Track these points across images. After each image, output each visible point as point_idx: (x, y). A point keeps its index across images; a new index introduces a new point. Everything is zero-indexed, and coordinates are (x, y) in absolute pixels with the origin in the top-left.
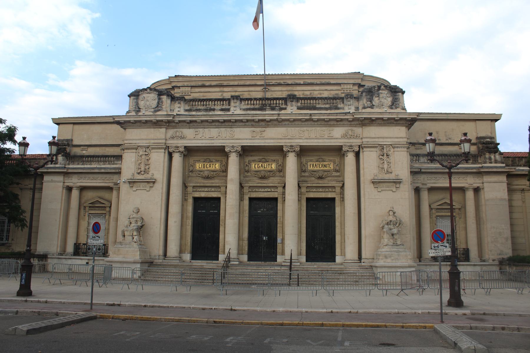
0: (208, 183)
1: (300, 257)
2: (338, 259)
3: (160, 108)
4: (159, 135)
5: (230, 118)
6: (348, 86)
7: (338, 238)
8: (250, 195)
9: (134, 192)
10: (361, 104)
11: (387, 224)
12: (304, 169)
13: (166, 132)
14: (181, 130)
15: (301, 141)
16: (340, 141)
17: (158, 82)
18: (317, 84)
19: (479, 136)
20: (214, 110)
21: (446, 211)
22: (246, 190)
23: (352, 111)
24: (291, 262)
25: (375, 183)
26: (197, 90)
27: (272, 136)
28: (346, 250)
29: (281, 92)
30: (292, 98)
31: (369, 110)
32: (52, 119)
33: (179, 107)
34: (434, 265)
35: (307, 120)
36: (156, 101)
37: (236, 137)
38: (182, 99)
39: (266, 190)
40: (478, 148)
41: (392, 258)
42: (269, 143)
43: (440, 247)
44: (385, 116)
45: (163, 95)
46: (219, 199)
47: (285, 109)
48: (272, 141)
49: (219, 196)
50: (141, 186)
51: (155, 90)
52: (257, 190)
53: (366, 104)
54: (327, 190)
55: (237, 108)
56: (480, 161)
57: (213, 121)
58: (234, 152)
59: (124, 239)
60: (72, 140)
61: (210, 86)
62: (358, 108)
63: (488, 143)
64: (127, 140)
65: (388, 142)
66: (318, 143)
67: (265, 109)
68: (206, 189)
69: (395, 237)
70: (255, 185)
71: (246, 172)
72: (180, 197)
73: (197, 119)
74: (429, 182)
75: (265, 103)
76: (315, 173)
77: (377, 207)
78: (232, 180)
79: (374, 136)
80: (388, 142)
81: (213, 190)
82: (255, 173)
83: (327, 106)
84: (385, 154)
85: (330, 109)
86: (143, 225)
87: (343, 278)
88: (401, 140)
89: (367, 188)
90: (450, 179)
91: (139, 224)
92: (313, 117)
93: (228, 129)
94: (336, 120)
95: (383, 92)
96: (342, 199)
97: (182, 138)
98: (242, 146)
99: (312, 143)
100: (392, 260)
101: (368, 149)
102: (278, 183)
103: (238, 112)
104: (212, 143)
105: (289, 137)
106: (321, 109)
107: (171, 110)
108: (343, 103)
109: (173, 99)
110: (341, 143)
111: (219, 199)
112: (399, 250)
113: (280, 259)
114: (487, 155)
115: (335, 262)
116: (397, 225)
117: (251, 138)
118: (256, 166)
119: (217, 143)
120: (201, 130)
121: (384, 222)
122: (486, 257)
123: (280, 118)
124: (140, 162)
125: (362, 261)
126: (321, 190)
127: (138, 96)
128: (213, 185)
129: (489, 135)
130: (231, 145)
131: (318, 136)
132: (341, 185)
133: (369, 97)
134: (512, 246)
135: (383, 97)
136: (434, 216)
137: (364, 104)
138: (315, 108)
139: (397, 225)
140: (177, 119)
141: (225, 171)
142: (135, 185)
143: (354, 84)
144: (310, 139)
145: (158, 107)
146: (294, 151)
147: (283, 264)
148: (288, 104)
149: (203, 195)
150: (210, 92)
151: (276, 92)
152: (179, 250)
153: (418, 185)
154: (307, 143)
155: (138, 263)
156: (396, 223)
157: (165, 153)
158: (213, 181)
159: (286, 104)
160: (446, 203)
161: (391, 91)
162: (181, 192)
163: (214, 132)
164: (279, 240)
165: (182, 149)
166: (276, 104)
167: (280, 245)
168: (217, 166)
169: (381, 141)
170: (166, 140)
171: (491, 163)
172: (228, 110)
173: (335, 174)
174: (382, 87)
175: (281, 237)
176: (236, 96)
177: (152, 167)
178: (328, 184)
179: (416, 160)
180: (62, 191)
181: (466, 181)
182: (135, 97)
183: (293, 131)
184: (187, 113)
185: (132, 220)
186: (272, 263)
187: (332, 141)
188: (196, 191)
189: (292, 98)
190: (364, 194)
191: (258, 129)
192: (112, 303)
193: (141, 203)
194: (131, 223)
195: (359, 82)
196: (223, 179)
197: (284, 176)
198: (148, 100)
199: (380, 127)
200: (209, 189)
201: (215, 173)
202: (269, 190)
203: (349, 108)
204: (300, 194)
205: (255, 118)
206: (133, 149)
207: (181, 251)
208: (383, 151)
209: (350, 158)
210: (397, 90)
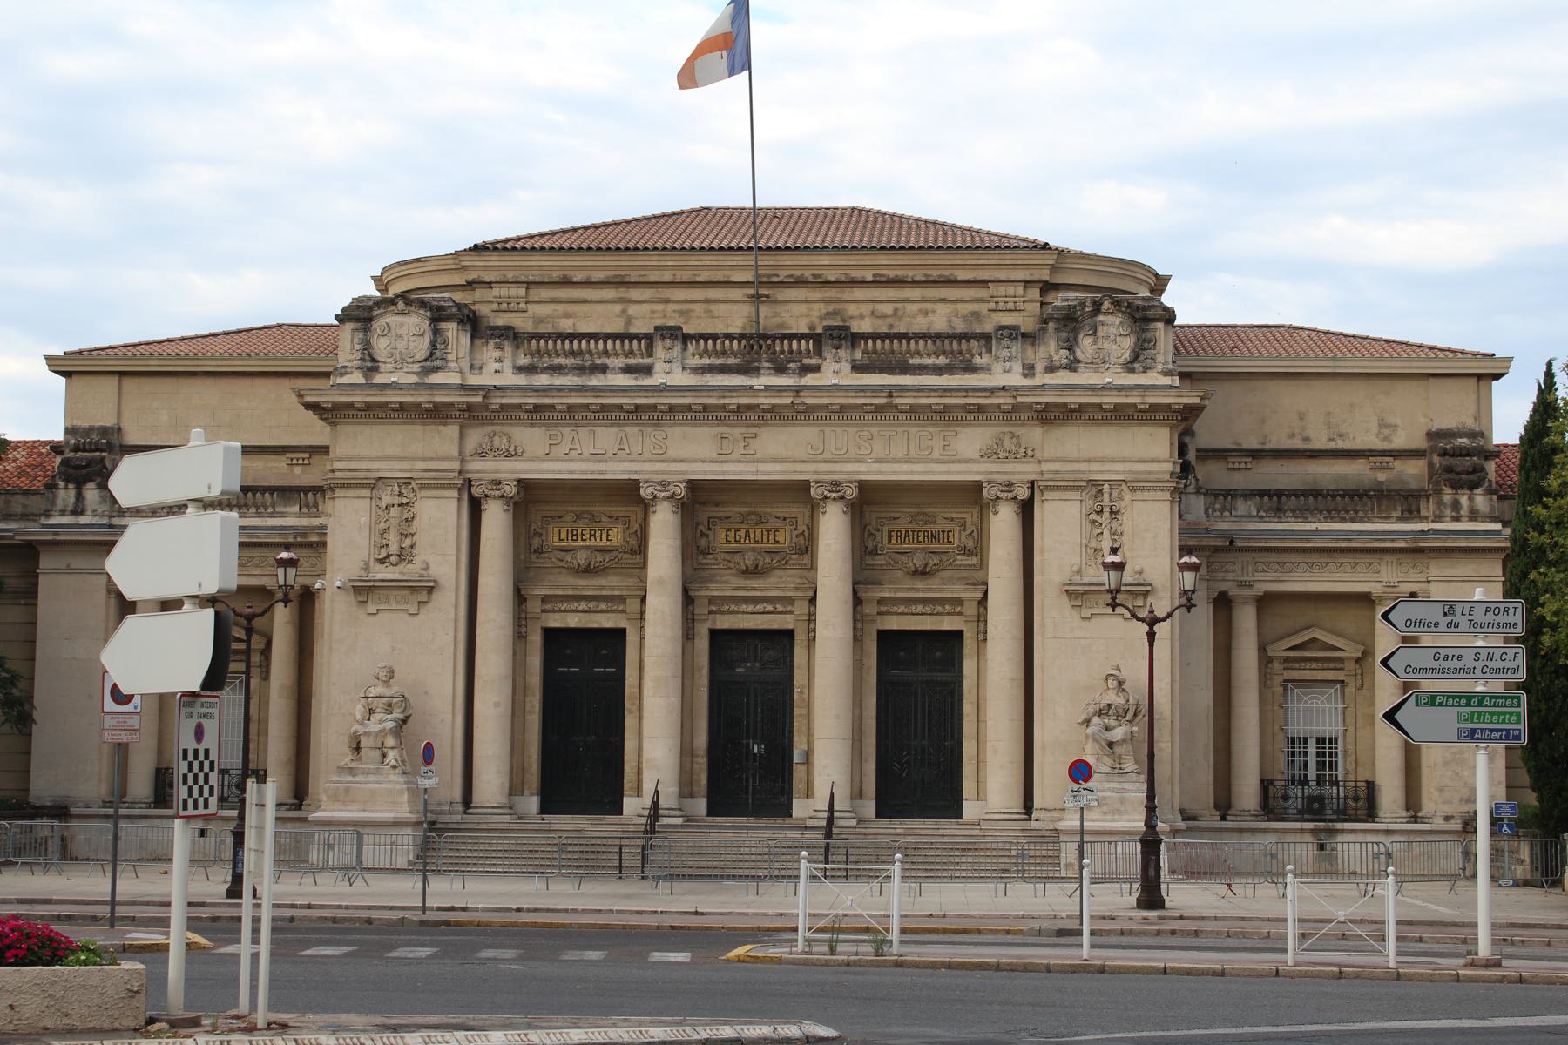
0: (589, 585)
2: (970, 809)
3: (438, 363)
4: (438, 446)
6: (1011, 291)
7: (969, 748)
9: (372, 619)
10: (1039, 356)
11: (1100, 713)
12: (871, 546)
13: (462, 436)
14: (506, 429)
15: (862, 467)
17: (418, 260)
18: (915, 283)
19: (1436, 426)
20: (604, 369)
23: (1015, 379)
24: (830, 820)
25: (1077, 594)
26: (546, 293)
27: (776, 455)
28: (990, 787)
30: (841, 336)
32: (48, 358)
33: (499, 360)
35: (878, 409)
36: (428, 338)
37: (671, 453)
38: (508, 335)
39: (760, 607)
40: (1431, 465)
41: (1105, 808)
42: (769, 473)
44: (1105, 400)
45: (448, 318)
46: (620, 633)
47: (816, 369)
48: (778, 467)
49: (622, 625)
51: (423, 304)
53: (1056, 358)
55: (674, 365)
56: (1424, 513)
57: (604, 408)
58: (665, 498)
61: (587, 283)
62: (1032, 367)
64: (340, 460)
66: (912, 473)
68: (583, 606)
69: (1118, 750)
70: (728, 593)
71: (703, 553)
72: (509, 630)
73: (555, 401)
74: (1259, 576)
75: (758, 348)
76: (904, 559)
77: (1075, 663)
78: (660, 582)
79: (1074, 454)
80: (1116, 471)
81: (603, 606)
82: (728, 557)
83: (942, 361)
84: (1107, 510)
88: (1155, 467)
89: (1051, 610)
91: (397, 714)
92: (898, 401)
94: (966, 408)
97: (511, 455)
98: (689, 481)
101: (1057, 495)
103: (680, 378)
104: (601, 472)
105: (827, 456)
108: (989, 351)
109: (472, 322)
110: (978, 473)
111: (620, 633)
112: (1126, 786)
113: (800, 808)
114: (1448, 495)
116: (1129, 716)
117: (714, 456)
118: (731, 534)
119: (617, 471)
120: (566, 430)
121: (1091, 710)
122: (1428, 807)
124: (383, 525)
126: (920, 608)
127: (370, 320)
128: (604, 593)
129: (1470, 423)
130: (660, 477)
132: (980, 595)
133: (1065, 335)
136: (1277, 680)
138: (906, 369)
139: (1129, 716)
140: (497, 401)
141: (641, 549)
143: (1027, 284)
145: (434, 359)
146: (842, 498)
147: (810, 823)
148: (825, 354)
149: (573, 621)
150: (585, 302)
152: (507, 785)
153: (1223, 587)
154: (879, 473)
158: (601, 581)
159: (819, 354)
160: (1314, 640)
165: (510, 490)
166: (791, 352)
167: (803, 768)
168: (616, 535)
169: (1097, 472)
170: (463, 461)
171: (1457, 519)
172: (648, 370)
173: (962, 560)
174: (1106, 305)
177: (422, 541)
178: (940, 591)
179: (1223, 509)
180: (107, 604)
182: (358, 325)
183: (840, 437)
184: (521, 380)
186: (779, 820)
188: (553, 611)
189: (841, 336)
193: (393, 649)
194: (371, 711)
195: (1046, 278)
196: (632, 576)
197: (813, 567)
198: (400, 336)
200: (592, 605)
201: (607, 557)
202: (770, 608)
203: (1003, 373)
205: (727, 401)
206: (363, 486)
207: (515, 789)
208: (1101, 498)
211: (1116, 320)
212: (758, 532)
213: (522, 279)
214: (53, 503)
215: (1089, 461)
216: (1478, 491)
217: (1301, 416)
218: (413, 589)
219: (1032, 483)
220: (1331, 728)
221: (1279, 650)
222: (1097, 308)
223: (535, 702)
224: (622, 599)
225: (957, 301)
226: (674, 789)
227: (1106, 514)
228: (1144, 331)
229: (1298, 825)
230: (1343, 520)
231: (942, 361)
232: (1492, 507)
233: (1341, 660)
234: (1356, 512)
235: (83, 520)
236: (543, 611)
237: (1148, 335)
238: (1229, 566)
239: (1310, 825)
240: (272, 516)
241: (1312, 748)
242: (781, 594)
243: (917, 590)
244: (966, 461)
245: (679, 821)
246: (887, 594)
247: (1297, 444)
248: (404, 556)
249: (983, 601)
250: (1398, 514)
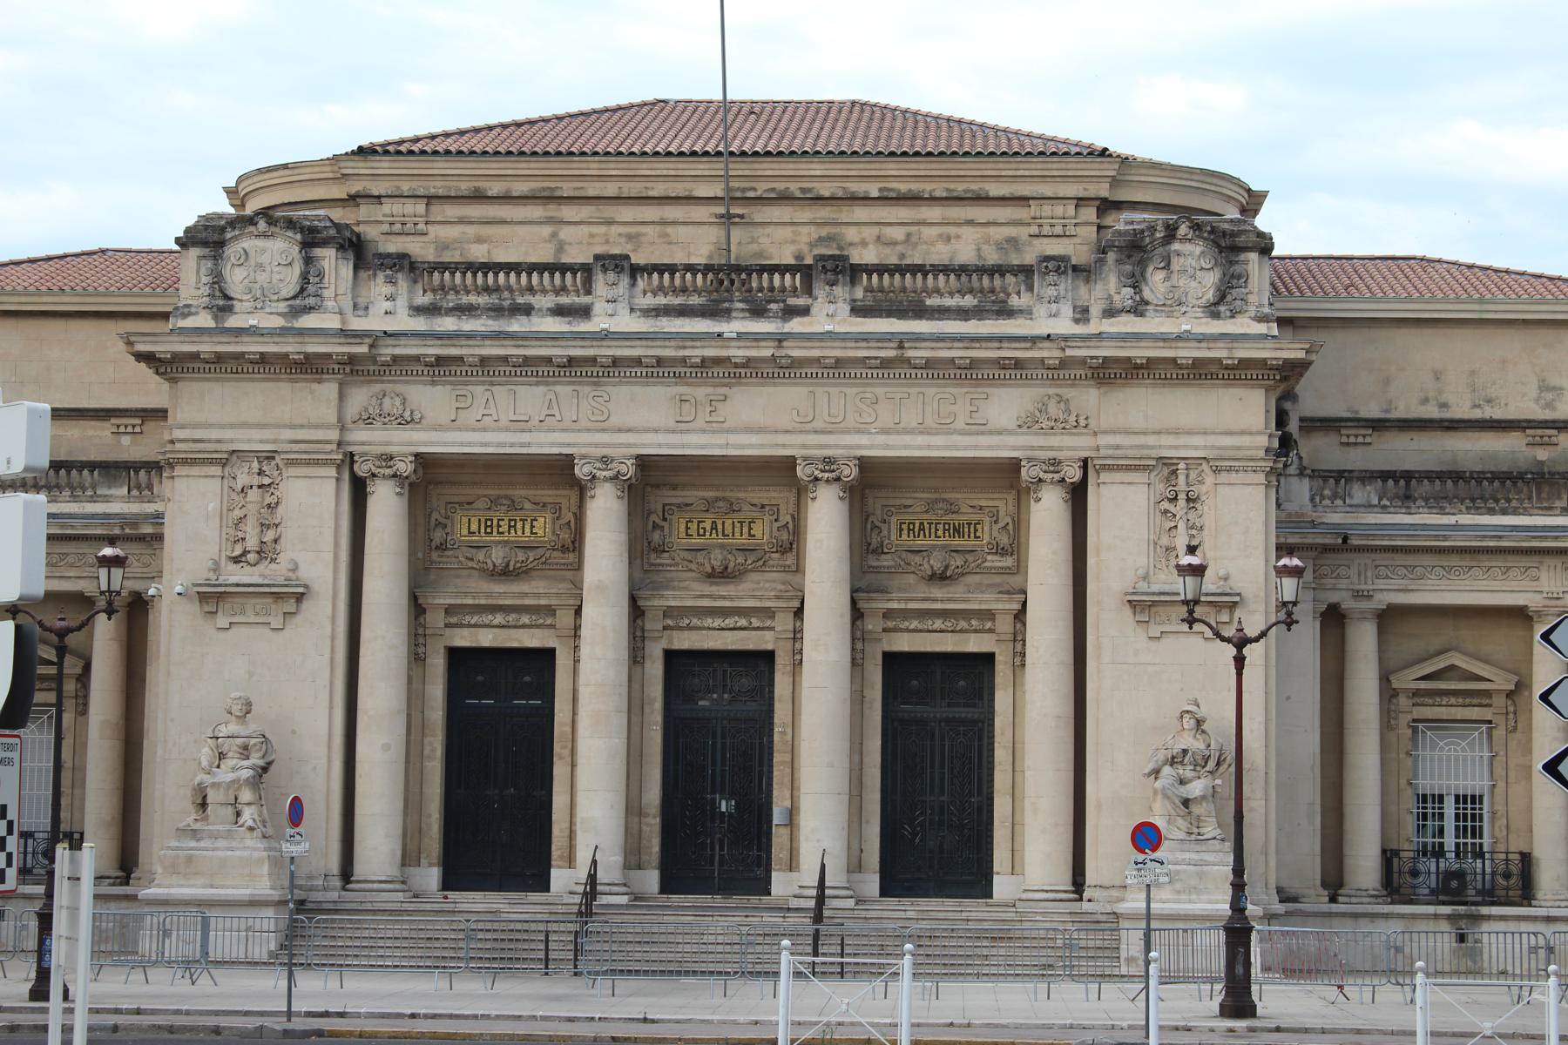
0: (506, 592)
1: (857, 876)
2: (1002, 886)
3: (311, 301)
4: (312, 408)
6: (1059, 210)
8: (671, 642)
9: (222, 635)
11: (1172, 761)
12: (875, 541)
13: (342, 397)
14: (400, 388)
15: (864, 440)
16: (1011, 440)
17: (285, 166)
18: (933, 199)
20: (527, 310)
21: (1453, 700)
22: (652, 624)
23: (1063, 325)
24: (821, 899)
25: (1142, 606)
26: (452, 211)
27: (752, 422)
28: (1028, 855)
31: (1126, 324)
34: (1387, 916)
35: (885, 363)
36: (297, 269)
37: (615, 420)
39: (729, 622)
41: (1178, 886)
42: (743, 447)
43: (1150, 864)
45: (324, 243)
47: (805, 311)
48: (754, 439)
49: (550, 644)
50: (250, 611)
51: (291, 224)
52: (695, 622)
53: (1116, 298)
54: (963, 624)
57: (527, 361)
58: (606, 479)
59: (206, 819)
61: (506, 198)
62: (1086, 310)
64: (182, 427)
65: (1196, 448)
66: (929, 447)
67: (728, 311)
68: (499, 619)
69: (1196, 809)
70: (689, 603)
74: (1380, 584)
76: (918, 559)
78: (601, 587)
80: (1194, 446)
81: (525, 619)
82: (689, 556)
83: (969, 301)
84: (1182, 496)
85: (977, 313)
86: (269, 763)
89: (1109, 624)
91: (256, 760)
92: (910, 353)
93: (587, 389)
95: (1186, 248)
96: (1018, 660)
98: (638, 457)
99: (906, 447)
100: (1179, 892)
101: (1118, 476)
102: (778, 598)
103: (626, 322)
104: (522, 445)
105: (818, 424)
106: (942, 313)
107: (355, 306)
108: (1030, 288)
109: (355, 248)
110: (1014, 448)
113: (781, 884)
115: (991, 896)
116: (1211, 765)
117: (671, 424)
118: (693, 526)
119: (545, 443)
121: (1161, 756)
123: (782, 353)
124: (238, 513)
125: (1086, 895)
126: (938, 624)
127: (221, 244)
128: (527, 602)
131: (930, 421)
132: (1017, 606)
133: (1128, 268)
136: (1404, 719)
137: (1110, 298)
139: (1211, 765)
140: (387, 351)
141: (575, 544)
142: (226, 605)
143: (1080, 201)
144: (898, 433)
145: (305, 296)
146: (838, 479)
147: (794, 903)
148: (816, 292)
149: (486, 639)
151: (769, 230)
152: (399, 853)
153: (1334, 597)
154: (887, 447)
156: (1207, 760)
157: (338, 480)
159: (809, 291)
160: (1452, 668)
161: (1218, 246)
162: (405, 631)
163: (530, 398)
164: (778, 817)
166: (772, 289)
168: (543, 527)
169: (1168, 446)
170: (343, 429)
173: (994, 561)
174: (1183, 229)
175: (788, 803)
176: (614, 257)
177: (289, 534)
179: (1334, 497)
181: (1533, 585)
183: (835, 400)
184: (420, 324)
185: (227, 745)
186: (754, 900)
190: (1098, 647)
191: (701, 393)
193: (251, 674)
196: (563, 580)
197: (799, 569)
198: (260, 267)
199: (1166, 390)
200: (512, 618)
201: (531, 555)
202: (743, 622)
203: (1048, 317)
205: (687, 353)
206: (211, 462)
207: (409, 857)
209: (1047, 515)
211: (1197, 248)
212: (728, 523)
213: (421, 192)
218: (278, 597)
219: (1085, 462)
221: (1406, 680)
222: (1171, 233)
223: (436, 745)
224: (550, 610)
225: (988, 224)
227: (1182, 502)
228: (1232, 263)
229: (1430, 909)
230: (1492, 512)
231: (969, 301)
234: (1509, 501)
236: (447, 626)
237: (1237, 269)
239: (1447, 910)
240: (92, 500)
241: (1449, 809)
242: (758, 604)
243: (935, 600)
244: (1000, 433)
245: (624, 900)
246: (895, 605)
247: (1432, 412)
248: (265, 553)
249: (1020, 615)
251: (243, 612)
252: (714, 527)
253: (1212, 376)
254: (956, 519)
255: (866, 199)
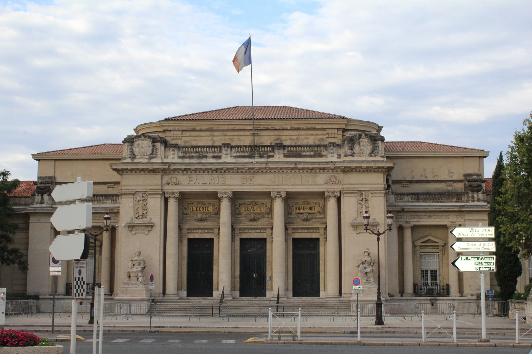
2: (322, 294)
3: (154, 155)
5: (221, 167)
6: (333, 131)
7: (321, 275)
11: (363, 263)
12: (290, 211)
13: (162, 178)
14: (176, 176)
15: (287, 187)
17: (148, 123)
18: (303, 129)
19: (466, 173)
20: (206, 157)
22: (237, 232)
23: (335, 159)
24: (278, 298)
26: (188, 133)
29: (269, 137)
30: (281, 146)
31: (350, 158)
32: (32, 155)
33: (173, 155)
35: (292, 169)
36: (151, 148)
37: (227, 183)
38: (176, 146)
39: (256, 231)
40: (465, 185)
41: (364, 293)
44: (363, 165)
45: (157, 142)
46: (212, 240)
47: (273, 156)
48: (261, 187)
49: (212, 237)
51: (149, 137)
52: (247, 231)
53: (347, 152)
54: (312, 231)
56: (463, 199)
59: (130, 280)
60: (55, 177)
62: (340, 155)
63: (476, 181)
66: (303, 189)
68: (200, 231)
69: (369, 275)
70: (246, 227)
74: (412, 220)
76: (300, 215)
81: (206, 231)
83: (312, 153)
84: (364, 200)
87: (325, 310)
88: (379, 186)
89: (346, 230)
90: (151, 317)
91: (142, 266)
92: (298, 166)
95: (364, 140)
97: (177, 184)
98: (233, 192)
103: (230, 160)
106: (305, 156)
108: (327, 150)
111: (212, 240)
113: (269, 294)
114: (470, 194)
115: (319, 296)
116: (372, 264)
117: (241, 184)
118: (246, 208)
119: (210, 189)
121: (360, 262)
122: (466, 292)
124: (137, 206)
126: (306, 231)
127: (133, 142)
129: (477, 172)
131: (303, 183)
132: (325, 227)
134: (491, 282)
135: (363, 146)
137: (346, 152)
138: (300, 156)
139: (372, 264)
140: (172, 167)
145: (153, 154)
146: (281, 197)
147: (272, 299)
149: (197, 236)
153: (401, 223)
155: (145, 300)
156: (371, 263)
159: (273, 151)
160: (429, 240)
163: (207, 178)
165: (177, 195)
166: (265, 151)
168: (210, 209)
170: (162, 186)
171: (473, 201)
172: (220, 157)
175: (270, 275)
176: (227, 144)
177: (150, 211)
179: (401, 199)
183: (280, 177)
184: (180, 161)
186: (262, 298)
187: (316, 187)
188: (191, 233)
191: (248, 176)
192: (158, 326)
193: (141, 245)
194: (134, 265)
197: (272, 218)
198: (142, 147)
200: (203, 231)
201: (208, 216)
202: (259, 231)
203: (331, 157)
204: (286, 234)
206: (131, 194)
207: (179, 289)
208: (362, 196)
209: (332, 204)
210: (377, 138)
211: (366, 140)
214: (34, 200)
215: (358, 184)
216: (480, 193)
217: (424, 170)
218: (147, 226)
219: (340, 192)
220: (435, 267)
221: (418, 243)
222: (360, 136)
223: (185, 262)
226: (283, 289)
228: (375, 144)
229: (425, 298)
230: (438, 202)
231: (312, 153)
232: (484, 198)
233: (438, 246)
235: (43, 205)
237: (376, 145)
238: (402, 217)
239: (429, 298)
240: (103, 204)
245: (231, 298)
247: (424, 179)
249: (325, 229)
250: (455, 200)
251: (138, 230)
252: (251, 208)
253: (371, 171)
254: (309, 206)
255: (287, 129)
